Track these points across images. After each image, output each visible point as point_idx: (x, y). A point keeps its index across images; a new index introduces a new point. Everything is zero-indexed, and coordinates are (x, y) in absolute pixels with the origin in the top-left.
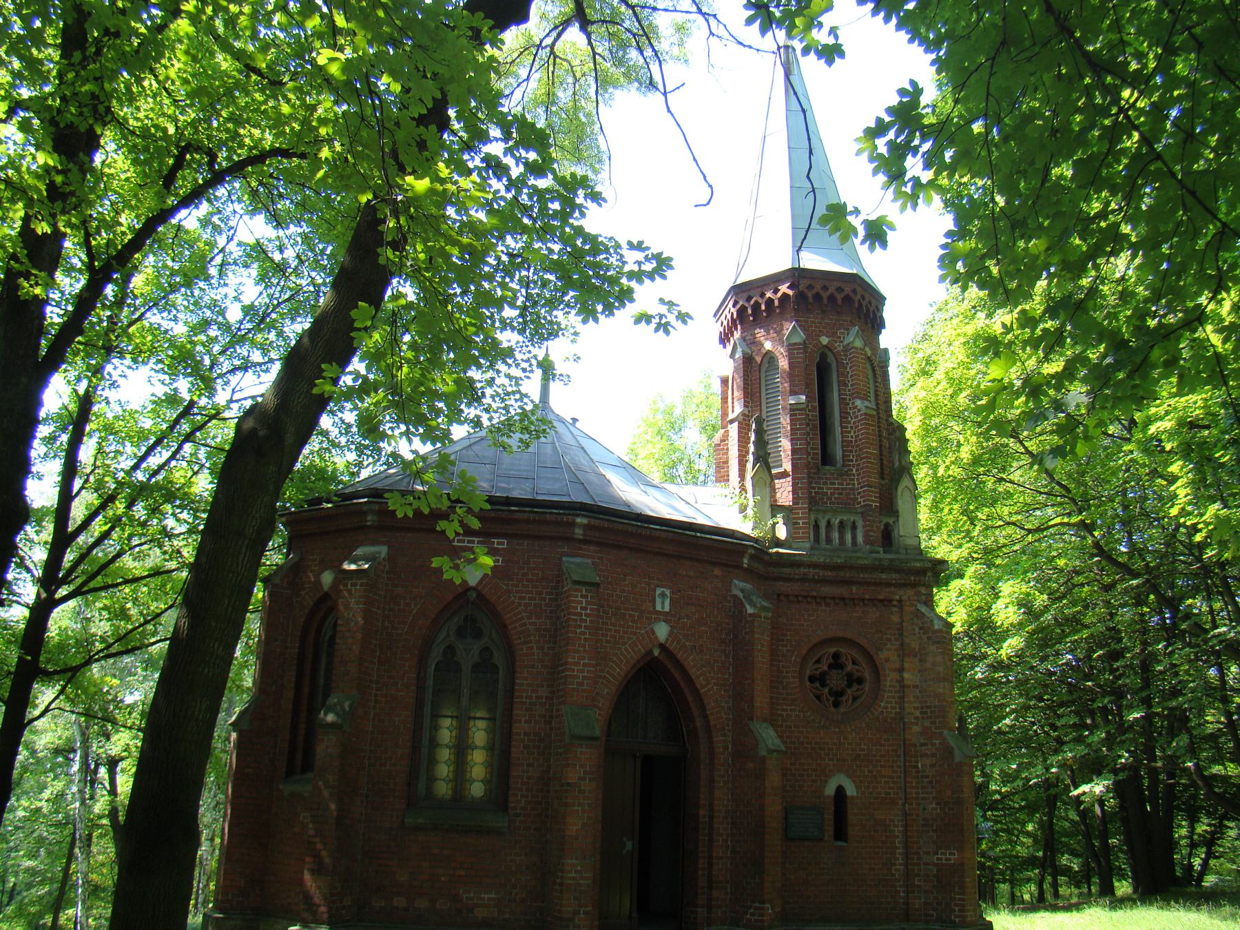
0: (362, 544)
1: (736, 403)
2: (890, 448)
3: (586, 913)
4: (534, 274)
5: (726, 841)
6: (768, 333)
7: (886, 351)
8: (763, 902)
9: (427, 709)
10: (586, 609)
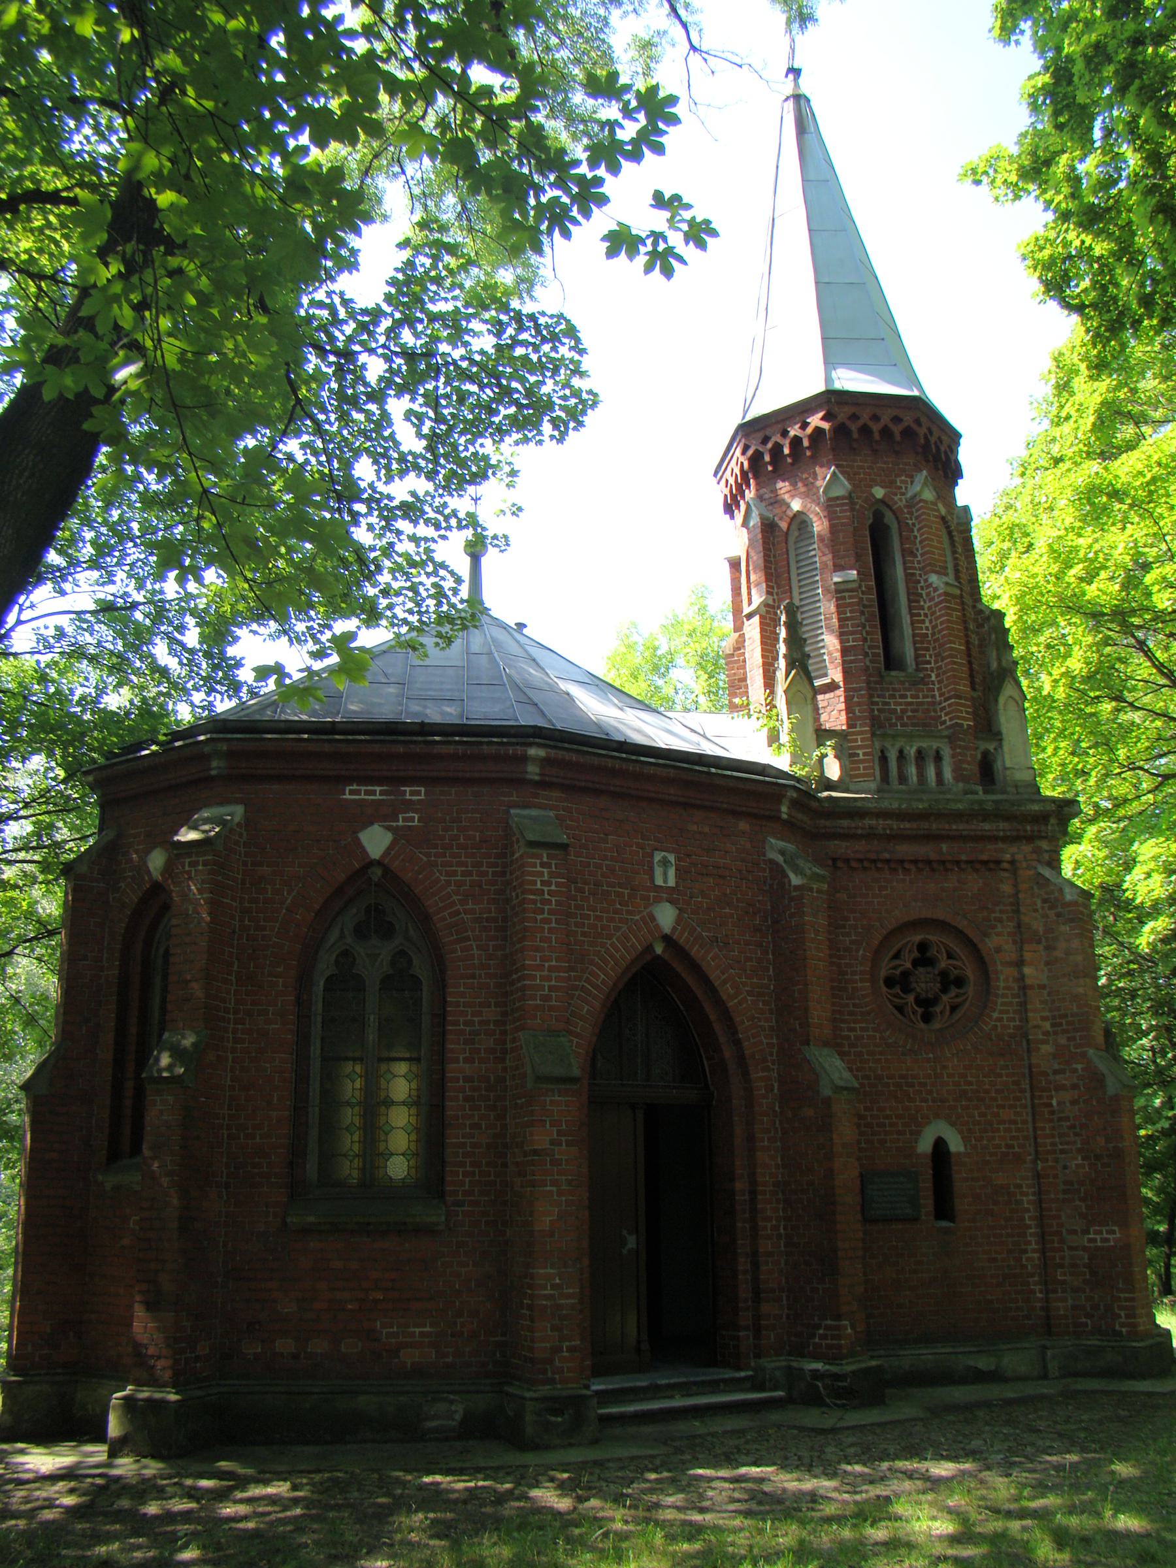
0: (207, 805)
1: (754, 591)
2: (980, 646)
3: (571, 1349)
4: (446, 384)
5: (776, 1228)
6: (794, 484)
7: (966, 509)
8: (838, 1317)
9: (315, 1050)
10: (549, 883)
